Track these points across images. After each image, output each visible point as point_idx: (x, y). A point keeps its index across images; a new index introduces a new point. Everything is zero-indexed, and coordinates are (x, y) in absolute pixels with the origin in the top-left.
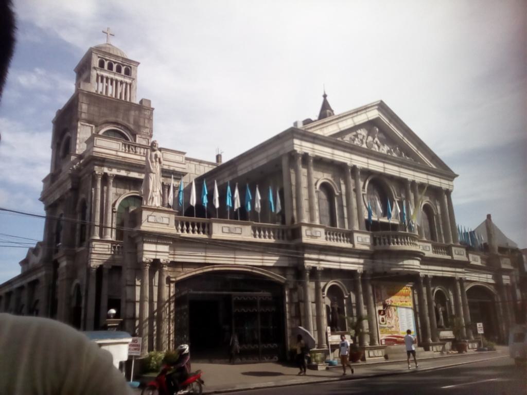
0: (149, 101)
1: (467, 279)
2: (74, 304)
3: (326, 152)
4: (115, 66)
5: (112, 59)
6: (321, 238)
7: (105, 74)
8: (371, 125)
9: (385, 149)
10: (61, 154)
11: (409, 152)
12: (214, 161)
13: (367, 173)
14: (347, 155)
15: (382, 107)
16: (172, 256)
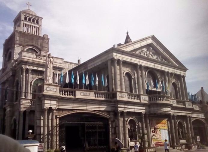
0: (47, 35)
1: (192, 116)
2: (13, 127)
3: (128, 59)
4: (32, 19)
5: (30, 16)
6: (126, 98)
7: (27, 23)
8: (148, 46)
9: (155, 57)
10: (7, 59)
11: (166, 59)
12: (77, 63)
13: (147, 68)
14: (138, 60)
15: (153, 38)
16: (58, 106)
